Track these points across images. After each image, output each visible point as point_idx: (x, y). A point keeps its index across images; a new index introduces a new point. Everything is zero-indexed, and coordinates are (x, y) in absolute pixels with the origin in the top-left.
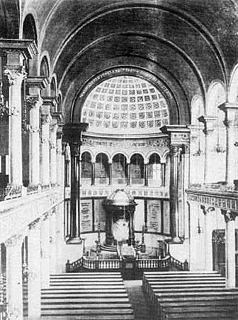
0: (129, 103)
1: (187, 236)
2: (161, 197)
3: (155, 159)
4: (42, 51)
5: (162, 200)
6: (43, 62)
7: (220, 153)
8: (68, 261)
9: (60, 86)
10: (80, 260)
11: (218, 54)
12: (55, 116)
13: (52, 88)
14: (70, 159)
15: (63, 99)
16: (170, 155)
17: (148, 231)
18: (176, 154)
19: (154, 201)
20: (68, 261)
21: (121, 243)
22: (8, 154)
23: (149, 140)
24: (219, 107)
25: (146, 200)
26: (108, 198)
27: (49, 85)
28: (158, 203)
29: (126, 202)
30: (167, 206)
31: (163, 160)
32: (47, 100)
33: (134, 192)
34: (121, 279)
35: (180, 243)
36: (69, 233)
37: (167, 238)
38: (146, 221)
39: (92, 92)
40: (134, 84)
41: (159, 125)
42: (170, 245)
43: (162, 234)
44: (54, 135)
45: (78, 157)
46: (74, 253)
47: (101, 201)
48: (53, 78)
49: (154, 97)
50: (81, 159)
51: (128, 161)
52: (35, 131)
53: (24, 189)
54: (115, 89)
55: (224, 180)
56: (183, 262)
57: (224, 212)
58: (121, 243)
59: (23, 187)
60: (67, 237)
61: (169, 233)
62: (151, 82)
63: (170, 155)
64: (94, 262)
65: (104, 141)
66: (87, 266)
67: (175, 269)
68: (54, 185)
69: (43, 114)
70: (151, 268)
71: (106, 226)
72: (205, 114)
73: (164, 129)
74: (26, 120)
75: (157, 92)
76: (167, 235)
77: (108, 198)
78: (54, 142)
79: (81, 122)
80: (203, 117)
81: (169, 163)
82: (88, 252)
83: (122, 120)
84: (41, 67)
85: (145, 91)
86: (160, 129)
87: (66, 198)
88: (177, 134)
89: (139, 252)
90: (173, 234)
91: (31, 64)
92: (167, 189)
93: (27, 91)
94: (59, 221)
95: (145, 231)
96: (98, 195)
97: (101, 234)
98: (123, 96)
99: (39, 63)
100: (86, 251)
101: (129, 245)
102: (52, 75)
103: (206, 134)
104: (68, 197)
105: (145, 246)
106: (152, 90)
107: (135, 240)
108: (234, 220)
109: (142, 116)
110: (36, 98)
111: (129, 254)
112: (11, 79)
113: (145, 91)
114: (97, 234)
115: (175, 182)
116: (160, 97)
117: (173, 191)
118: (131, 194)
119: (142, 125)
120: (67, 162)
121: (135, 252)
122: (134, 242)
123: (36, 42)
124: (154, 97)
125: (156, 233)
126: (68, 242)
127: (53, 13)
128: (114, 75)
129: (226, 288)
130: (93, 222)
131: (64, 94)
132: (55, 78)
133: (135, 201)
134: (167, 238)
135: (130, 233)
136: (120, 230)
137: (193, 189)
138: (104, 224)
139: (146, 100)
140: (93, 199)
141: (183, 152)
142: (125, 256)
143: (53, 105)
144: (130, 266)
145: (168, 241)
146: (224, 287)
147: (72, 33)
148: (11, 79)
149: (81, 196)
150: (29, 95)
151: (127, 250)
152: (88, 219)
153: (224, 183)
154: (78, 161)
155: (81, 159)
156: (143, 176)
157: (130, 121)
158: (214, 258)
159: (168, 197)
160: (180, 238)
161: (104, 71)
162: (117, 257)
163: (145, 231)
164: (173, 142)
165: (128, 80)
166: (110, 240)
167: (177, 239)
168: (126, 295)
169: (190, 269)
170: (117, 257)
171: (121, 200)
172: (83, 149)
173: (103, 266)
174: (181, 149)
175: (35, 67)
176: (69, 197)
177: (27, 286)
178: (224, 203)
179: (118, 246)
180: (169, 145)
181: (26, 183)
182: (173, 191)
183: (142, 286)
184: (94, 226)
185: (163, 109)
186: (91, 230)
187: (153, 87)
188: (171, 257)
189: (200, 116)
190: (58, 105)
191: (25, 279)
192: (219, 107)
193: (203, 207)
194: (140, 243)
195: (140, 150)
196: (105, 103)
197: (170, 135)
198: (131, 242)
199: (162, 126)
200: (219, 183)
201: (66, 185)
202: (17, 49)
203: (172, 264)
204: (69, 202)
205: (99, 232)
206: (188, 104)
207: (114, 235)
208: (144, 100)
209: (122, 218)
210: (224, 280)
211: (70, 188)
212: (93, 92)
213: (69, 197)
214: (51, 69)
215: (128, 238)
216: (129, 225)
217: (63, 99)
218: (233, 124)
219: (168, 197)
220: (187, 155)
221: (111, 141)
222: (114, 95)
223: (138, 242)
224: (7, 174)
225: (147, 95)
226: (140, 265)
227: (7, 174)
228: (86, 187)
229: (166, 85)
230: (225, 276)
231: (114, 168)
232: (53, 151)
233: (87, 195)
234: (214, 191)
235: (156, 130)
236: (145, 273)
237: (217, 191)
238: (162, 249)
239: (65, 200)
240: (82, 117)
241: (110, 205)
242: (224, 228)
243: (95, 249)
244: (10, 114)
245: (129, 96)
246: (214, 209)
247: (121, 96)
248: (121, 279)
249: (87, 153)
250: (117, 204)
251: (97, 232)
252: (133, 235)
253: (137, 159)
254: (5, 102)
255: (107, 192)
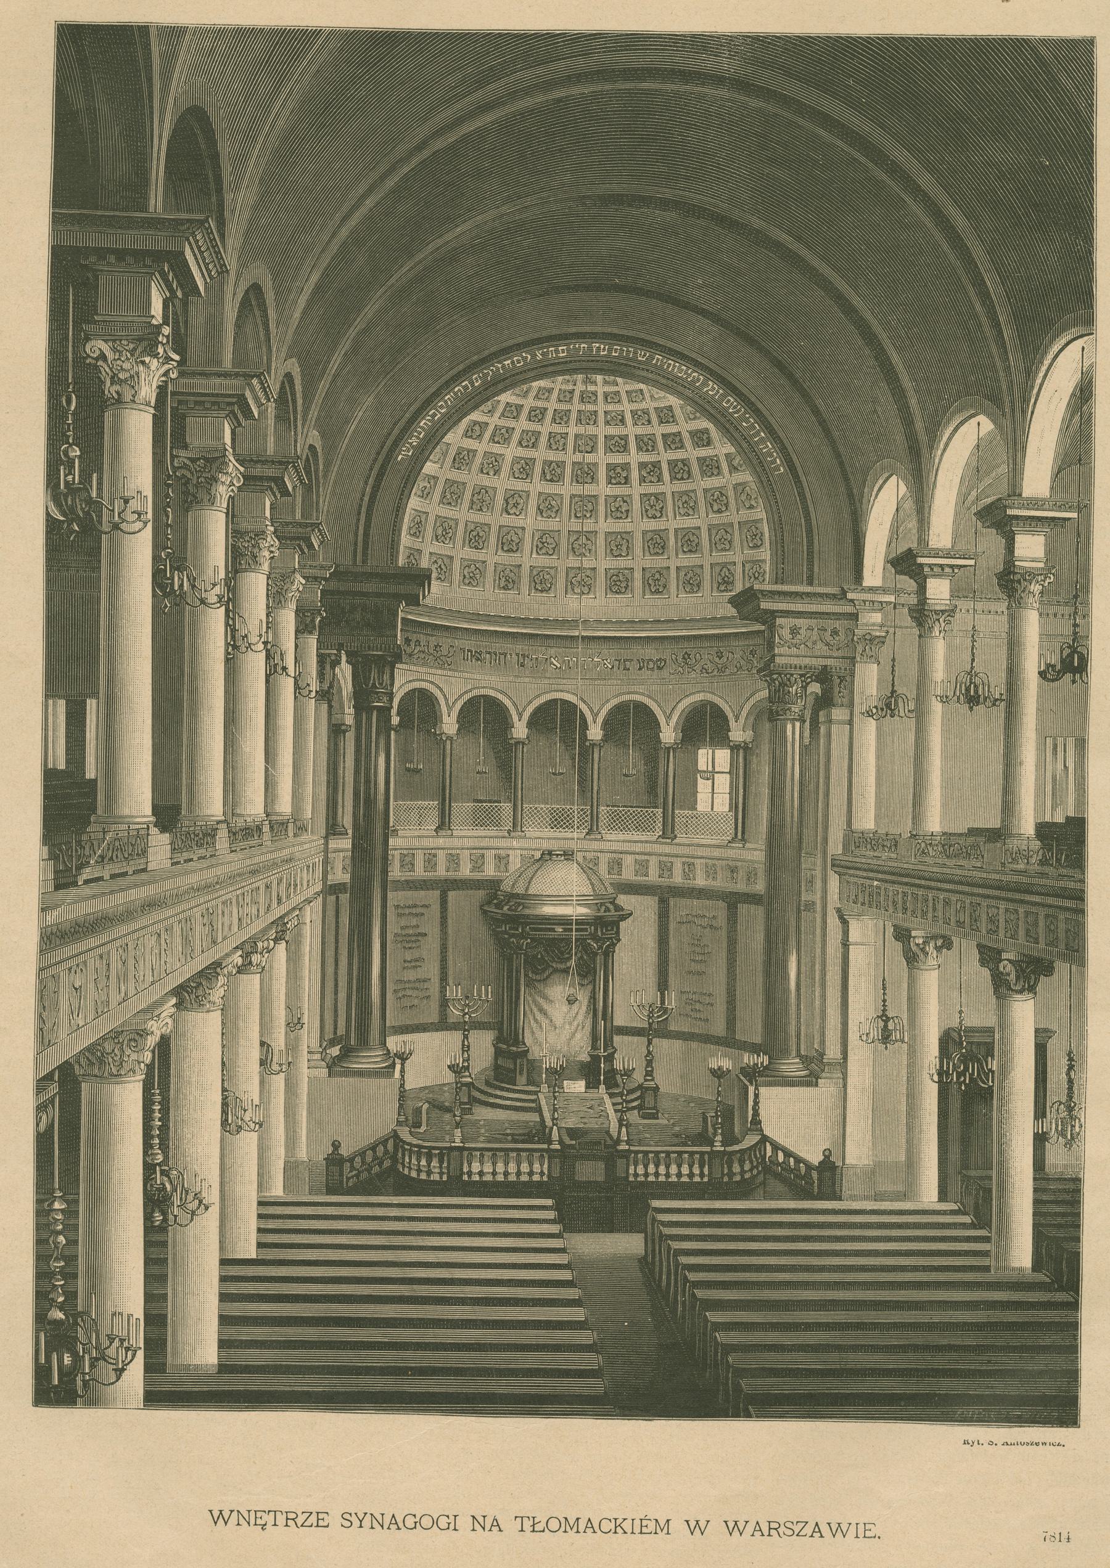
0: (602, 488)
1: (833, 1052)
2: (731, 887)
3: (704, 725)
4: (243, 265)
5: (733, 901)
6: (245, 304)
7: (980, 709)
8: (336, 1145)
9: (314, 413)
10: (384, 1142)
11: (985, 295)
12: (294, 537)
13: (285, 416)
14: (349, 718)
15: (328, 464)
16: (771, 714)
17: (673, 1027)
18: (796, 709)
19: (696, 905)
20: (336, 1145)
21: (558, 1075)
22: (95, 695)
23: (685, 647)
24: (980, 515)
25: (665, 896)
26: (506, 886)
27: (271, 407)
28: (720, 910)
29: (582, 900)
30: (753, 919)
31: (738, 734)
32: (258, 470)
33: (616, 865)
34: (555, 1229)
35: (809, 1084)
36: (341, 1031)
37: (748, 1059)
38: (663, 985)
39: (449, 438)
40: (627, 407)
41: (726, 583)
42: (763, 1090)
43: (729, 1042)
44: (288, 619)
45: (385, 712)
46: (366, 1115)
47: (481, 893)
48: (289, 376)
49: (710, 467)
50: (395, 720)
51: (595, 733)
52: (212, 598)
53: (160, 844)
54: (546, 428)
55: (995, 823)
56: (815, 1158)
57: (989, 956)
58: (558, 1075)
59: (154, 830)
60: (332, 1043)
61: (758, 1039)
62: (702, 406)
63: (771, 714)
64: (445, 1153)
65: (498, 646)
66: (413, 1167)
67: (780, 1187)
68: (284, 824)
69: (244, 526)
70: (691, 1185)
71: (499, 1002)
72: (923, 540)
73: (746, 601)
74: (173, 557)
75: (722, 448)
76: (755, 1049)
77: (506, 886)
78: (288, 643)
79: (401, 562)
80: (910, 555)
81: (765, 748)
82: (418, 1111)
83: (573, 562)
84: (238, 326)
85: (673, 441)
86: (733, 601)
87: (332, 879)
88: (801, 622)
89: (633, 1117)
90: (773, 1043)
91: (198, 318)
92: (755, 853)
93: (180, 420)
94: (287, 988)
95: (653, 1030)
96: (465, 871)
97: (474, 1036)
98: (578, 457)
99: (230, 313)
100: (410, 1104)
101: (592, 1085)
102: (283, 365)
103: (920, 624)
104: (341, 875)
105: (656, 1089)
106: (701, 438)
107: (618, 1065)
108: (1032, 989)
109: (656, 543)
110: (214, 461)
111: (593, 1124)
112: (114, 379)
113: (673, 441)
114: (457, 1036)
115: (790, 834)
116: (733, 469)
117: (785, 849)
118: (603, 869)
119: (655, 583)
120: (336, 731)
121: (613, 1117)
122: (611, 1073)
123: (221, 224)
124: (710, 467)
125: (707, 1039)
126: (334, 1067)
127: (290, 105)
128: (547, 370)
129: (991, 1276)
130: (444, 979)
131: (330, 448)
132: (298, 381)
133: (623, 900)
134: (748, 1059)
135: (595, 1038)
136: (558, 1024)
137: (866, 856)
138: (488, 993)
139: (673, 478)
140: (446, 886)
141: (825, 701)
142: (572, 1133)
143: (285, 492)
144: (591, 1171)
145: (752, 1074)
146: (987, 1269)
147: (370, 190)
148: (114, 379)
149: (396, 872)
150: (185, 447)
151: (578, 1103)
152: (421, 974)
153: (995, 835)
154: (385, 727)
155: (395, 720)
156: (660, 794)
157: (604, 563)
158: (328, 809)
159: (760, 887)
160: (806, 1060)
161: (506, 351)
162: (540, 1133)
163: (653, 1030)
164: (785, 656)
165: (601, 390)
166: (512, 1061)
167: (791, 1066)
168: (573, 1293)
169: (846, 1193)
170: (540, 1133)
171: (564, 894)
172: (405, 680)
173: (477, 1168)
174: (815, 688)
175: (214, 327)
176: (346, 878)
177: (164, 1244)
178: (991, 920)
179: (544, 1088)
180: (768, 670)
181: (167, 814)
182: (785, 849)
183: (643, 1261)
184: (444, 1003)
185: (745, 514)
186: (434, 1018)
187: (704, 424)
188: (765, 1139)
189: (902, 548)
190: (308, 489)
191: (158, 1217)
192: (980, 515)
193: (902, 935)
194: (638, 1077)
195: (641, 691)
196: (502, 483)
197: (772, 627)
198: (593, 1071)
199: (739, 587)
200: (973, 832)
201: (333, 829)
202: (139, 255)
203: (768, 1169)
204: (345, 898)
205: (464, 1027)
206: (850, 495)
207: (528, 1040)
208: (666, 476)
209: (566, 971)
210: (987, 1239)
211: (346, 843)
212: (454, 438)
213: (346, 878)
214: (282, 336)
215: (584, 1057)
216: (593, 998)
217: (328, 464)
218: (1036, 588)
219: (760, 887)
220: (838, 714)
221: (520, 647)
222: (542, 454)
223: (628, 1073)
224: (90, 774)
225: (679, 455)
226: (637, 1171)
227: (90, 774)
228: (415, 837)
229: (757, 412)
230: (988, 1225)
231: (542, 762)
232: (287, 686)
233: (420, 872)
234: (953, 867)
235: (710, 605)
236: (656, 1203)
237: (968, 867)
238: (731, 1115)
239: (332, 890)
240: (405, 540)
241: (515, 920)
242: (991, 1021)
243: (447, 1098)
244: (106, 527)
245: (602, 458)
246: (948, 944)
247: (570, 457)
248: (555, 1229)
249: (422, 692)
250: (548, 910)
251: (454, 1027)
252: (609, 1042)
253: (631, 722)
254: (86, 477)
255: (502, 860)
